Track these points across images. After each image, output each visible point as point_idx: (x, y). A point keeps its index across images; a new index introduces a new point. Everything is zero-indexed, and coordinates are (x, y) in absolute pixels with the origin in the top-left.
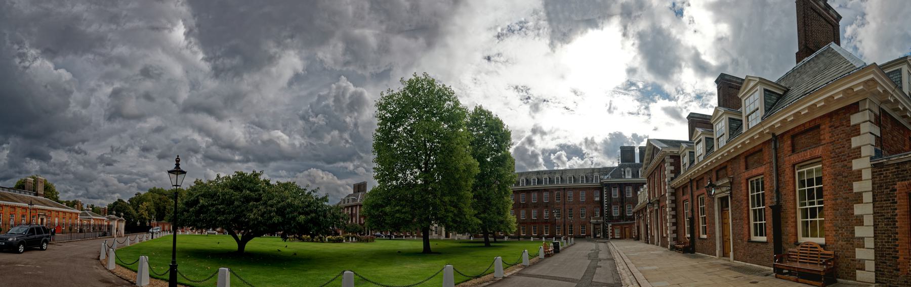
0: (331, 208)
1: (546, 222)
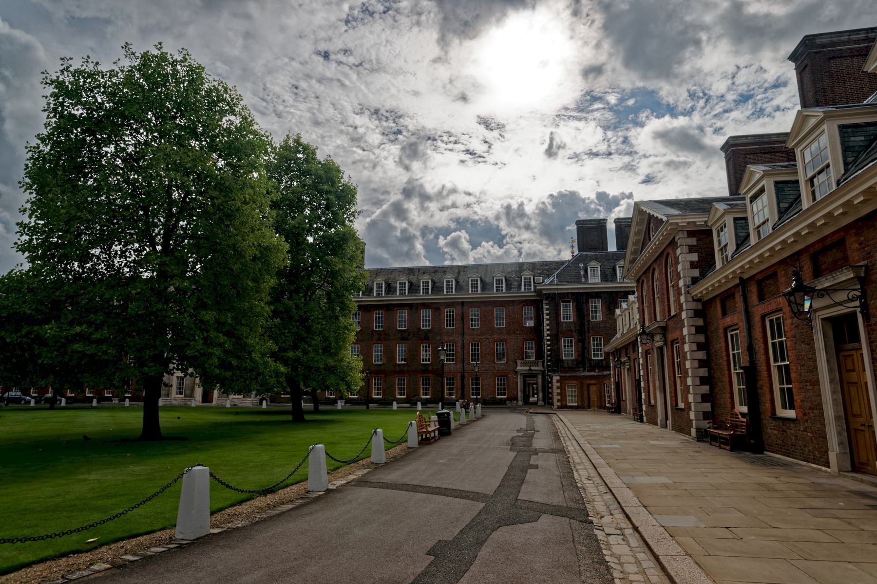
1: (425, 370)
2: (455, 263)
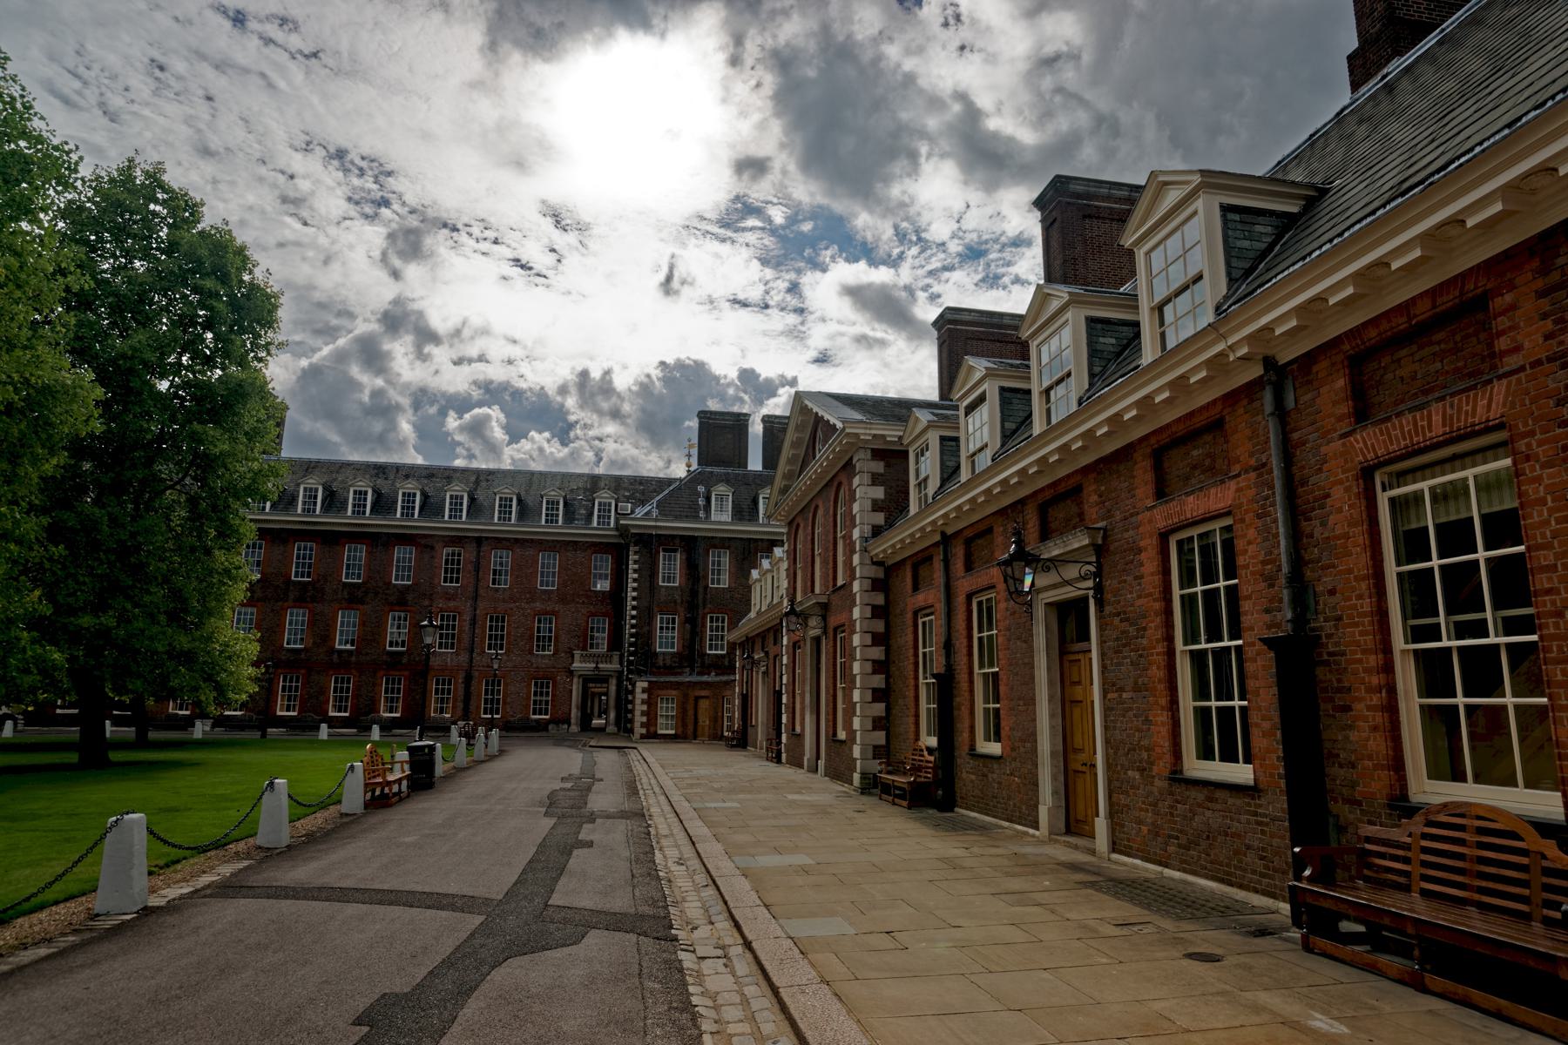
2: (475, 465)
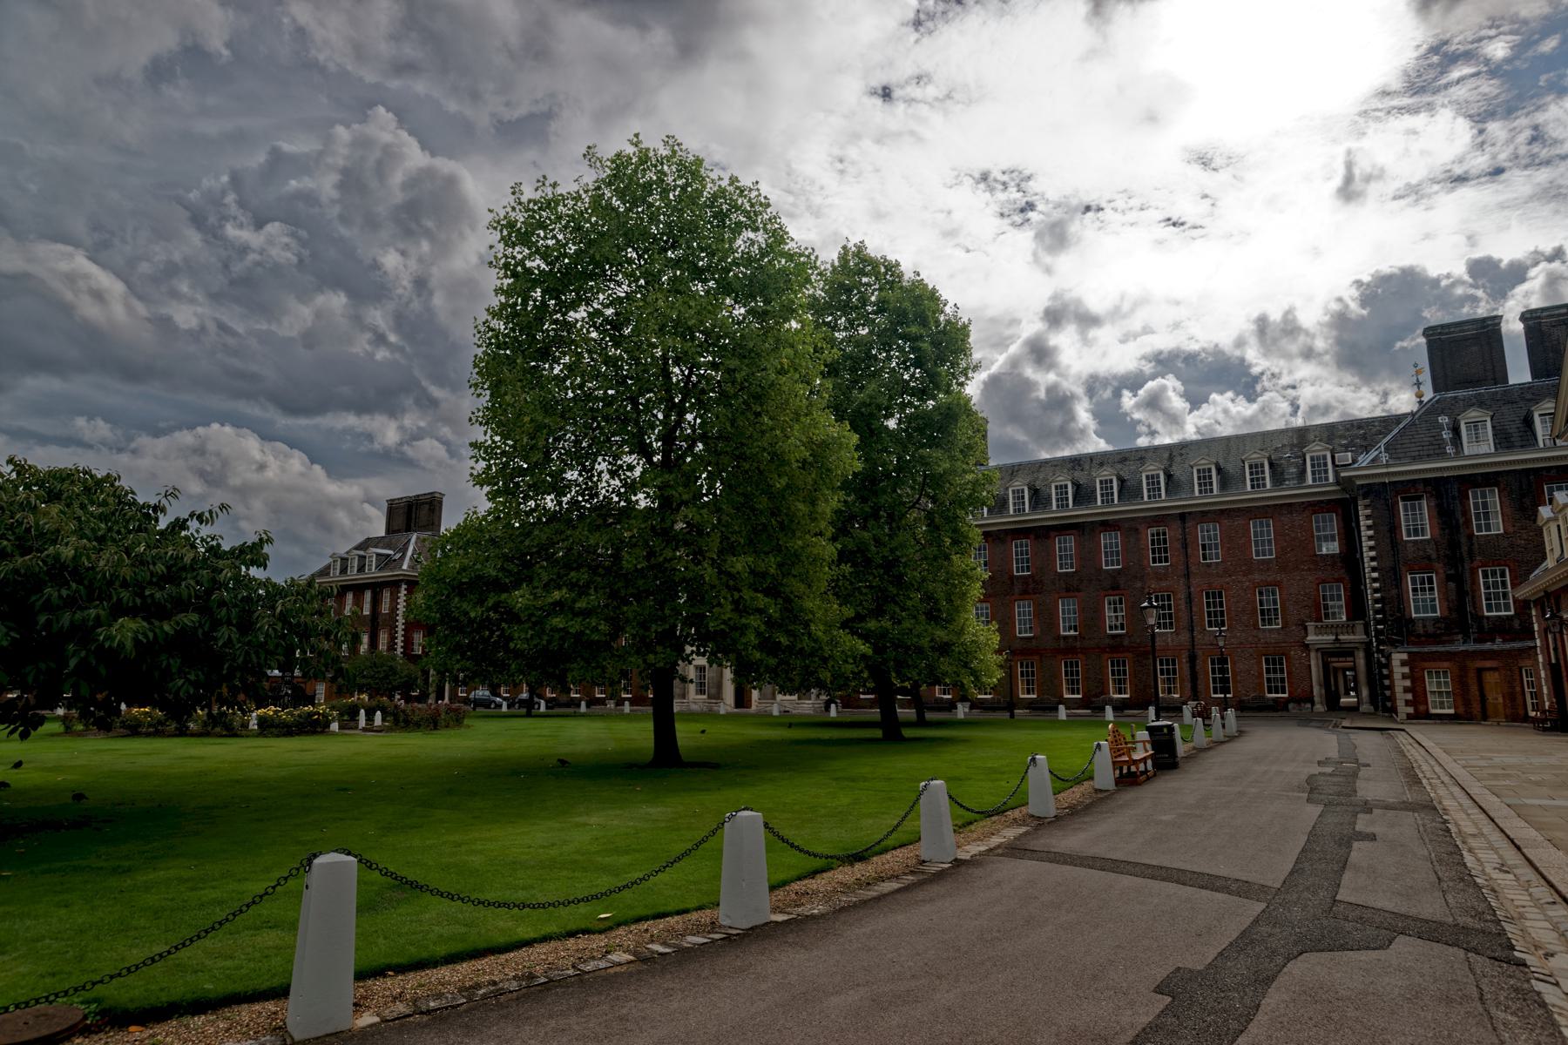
0: (275, 592)
2: (1158, 441)
